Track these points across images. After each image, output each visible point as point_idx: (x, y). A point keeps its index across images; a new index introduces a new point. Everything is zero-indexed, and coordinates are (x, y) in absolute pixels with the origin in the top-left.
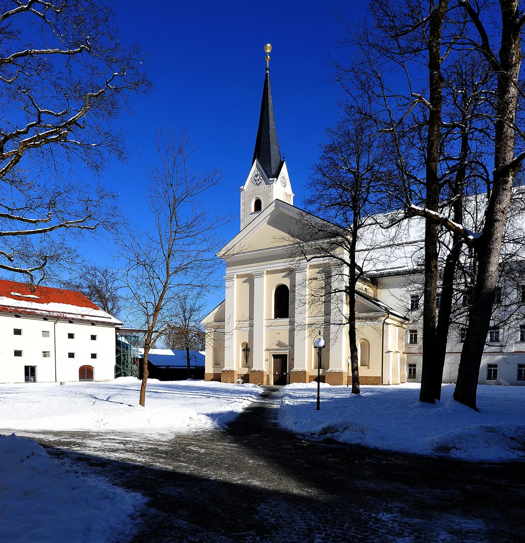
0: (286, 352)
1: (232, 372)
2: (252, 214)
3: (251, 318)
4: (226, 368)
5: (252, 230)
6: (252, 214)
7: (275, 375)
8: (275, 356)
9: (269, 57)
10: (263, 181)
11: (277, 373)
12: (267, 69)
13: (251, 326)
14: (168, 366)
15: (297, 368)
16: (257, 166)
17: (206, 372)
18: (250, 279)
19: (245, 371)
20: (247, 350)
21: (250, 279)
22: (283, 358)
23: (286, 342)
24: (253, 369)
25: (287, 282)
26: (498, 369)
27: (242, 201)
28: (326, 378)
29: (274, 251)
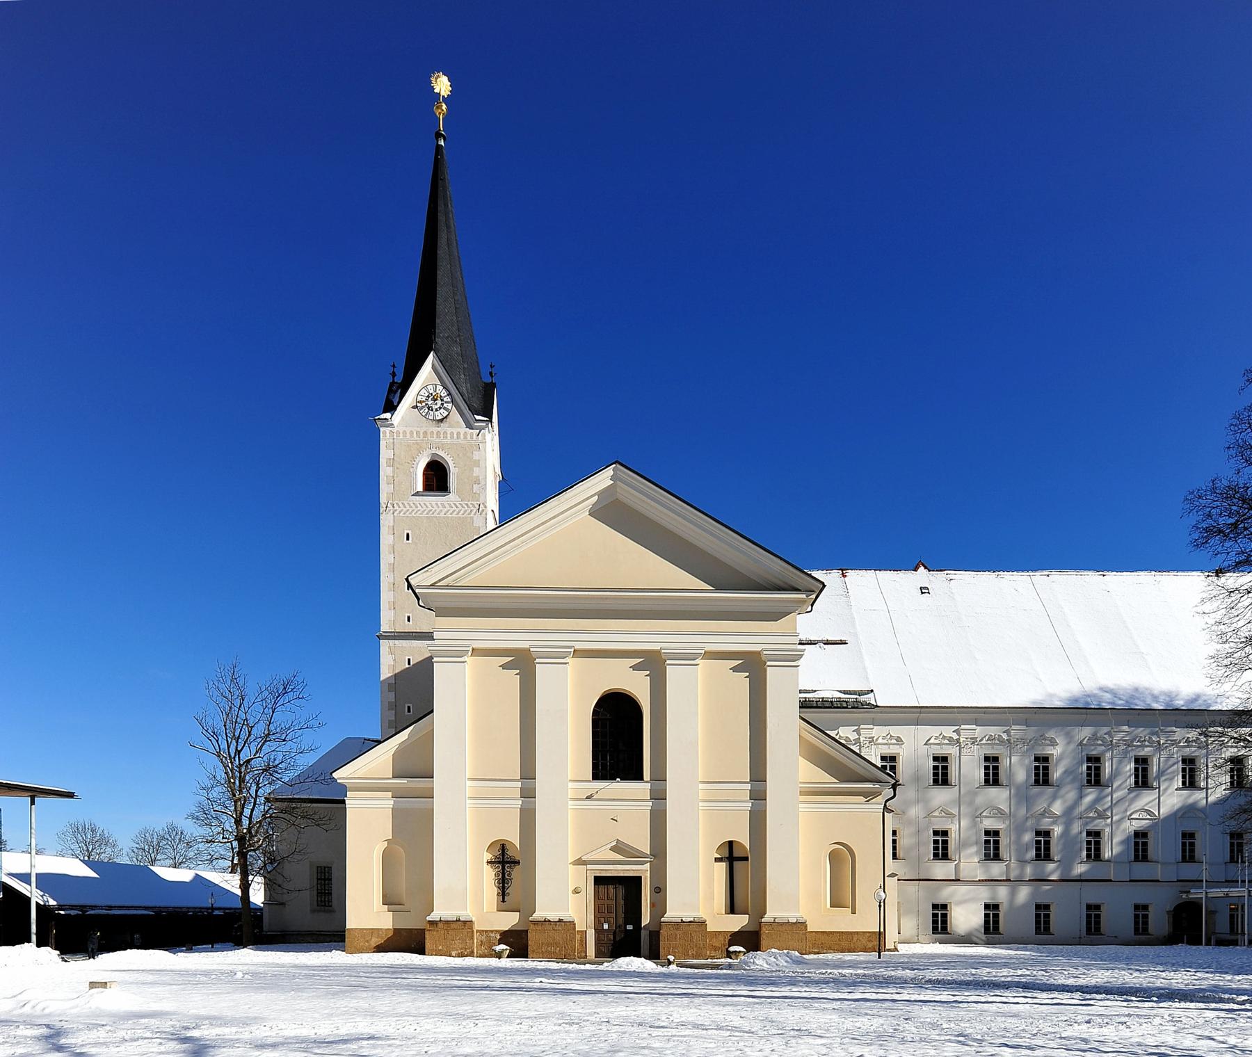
0: (643, 870)
1: (468, 924)
2: (417, 494)
3: (528, 773)
4: (440, 912)
5: (691, 522)
6: (417, 494)
7: (599, 931)
8: (599, 881)
9: (444, 107)
10: (455, 415)
11: (606, 926)
12: (438, 135)
13: (528, 794)
14: (82, 907)
15: (674, 912)
16: (434, 367)
17: (350, 925)
18: (522, 663)
19: (509, 921)
20: (508, 864)
21: (522, 663)
22: (632, 885)
23: (643, 844)
24: (539, 914)
25: (638, 687)
26: (1104, 913)
27: (385, 454)
28: (763, 936)
29: (601, 598)
